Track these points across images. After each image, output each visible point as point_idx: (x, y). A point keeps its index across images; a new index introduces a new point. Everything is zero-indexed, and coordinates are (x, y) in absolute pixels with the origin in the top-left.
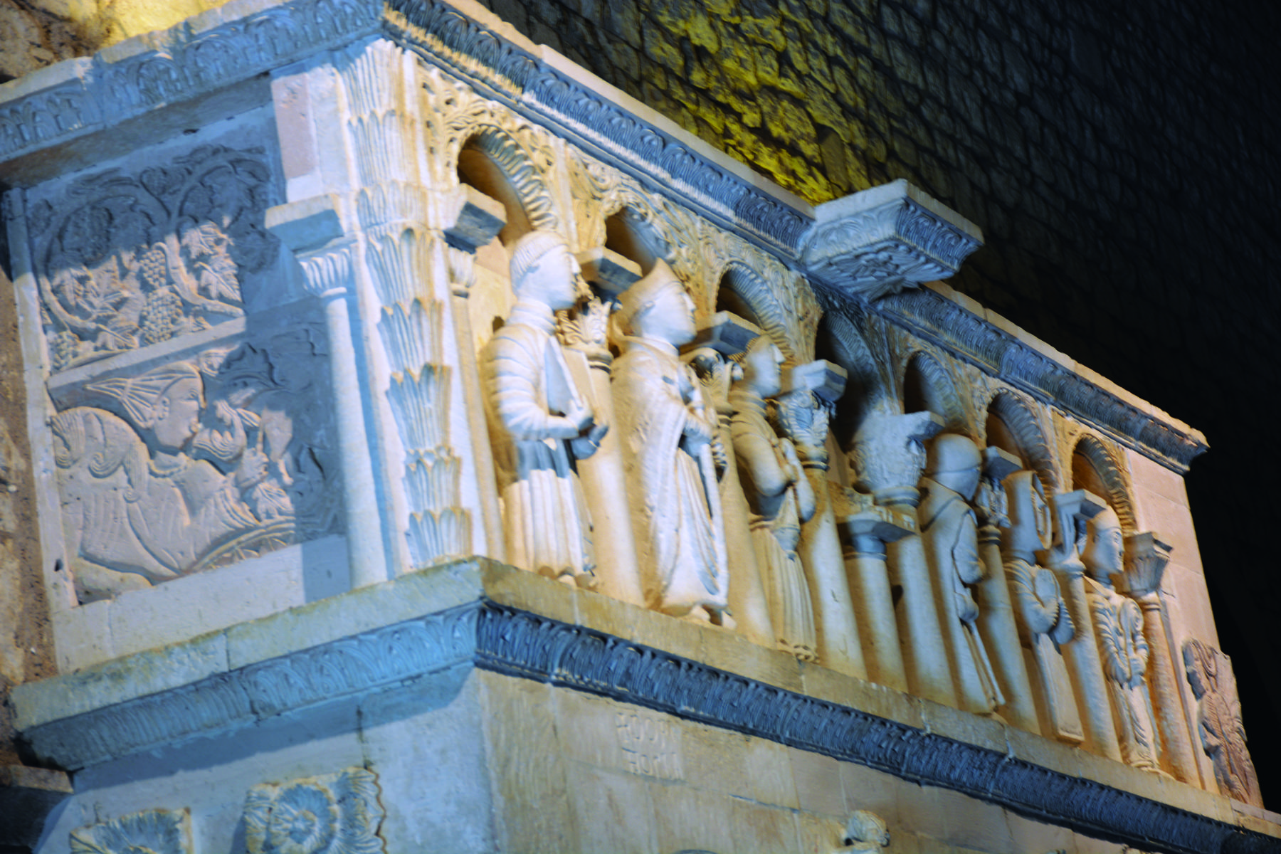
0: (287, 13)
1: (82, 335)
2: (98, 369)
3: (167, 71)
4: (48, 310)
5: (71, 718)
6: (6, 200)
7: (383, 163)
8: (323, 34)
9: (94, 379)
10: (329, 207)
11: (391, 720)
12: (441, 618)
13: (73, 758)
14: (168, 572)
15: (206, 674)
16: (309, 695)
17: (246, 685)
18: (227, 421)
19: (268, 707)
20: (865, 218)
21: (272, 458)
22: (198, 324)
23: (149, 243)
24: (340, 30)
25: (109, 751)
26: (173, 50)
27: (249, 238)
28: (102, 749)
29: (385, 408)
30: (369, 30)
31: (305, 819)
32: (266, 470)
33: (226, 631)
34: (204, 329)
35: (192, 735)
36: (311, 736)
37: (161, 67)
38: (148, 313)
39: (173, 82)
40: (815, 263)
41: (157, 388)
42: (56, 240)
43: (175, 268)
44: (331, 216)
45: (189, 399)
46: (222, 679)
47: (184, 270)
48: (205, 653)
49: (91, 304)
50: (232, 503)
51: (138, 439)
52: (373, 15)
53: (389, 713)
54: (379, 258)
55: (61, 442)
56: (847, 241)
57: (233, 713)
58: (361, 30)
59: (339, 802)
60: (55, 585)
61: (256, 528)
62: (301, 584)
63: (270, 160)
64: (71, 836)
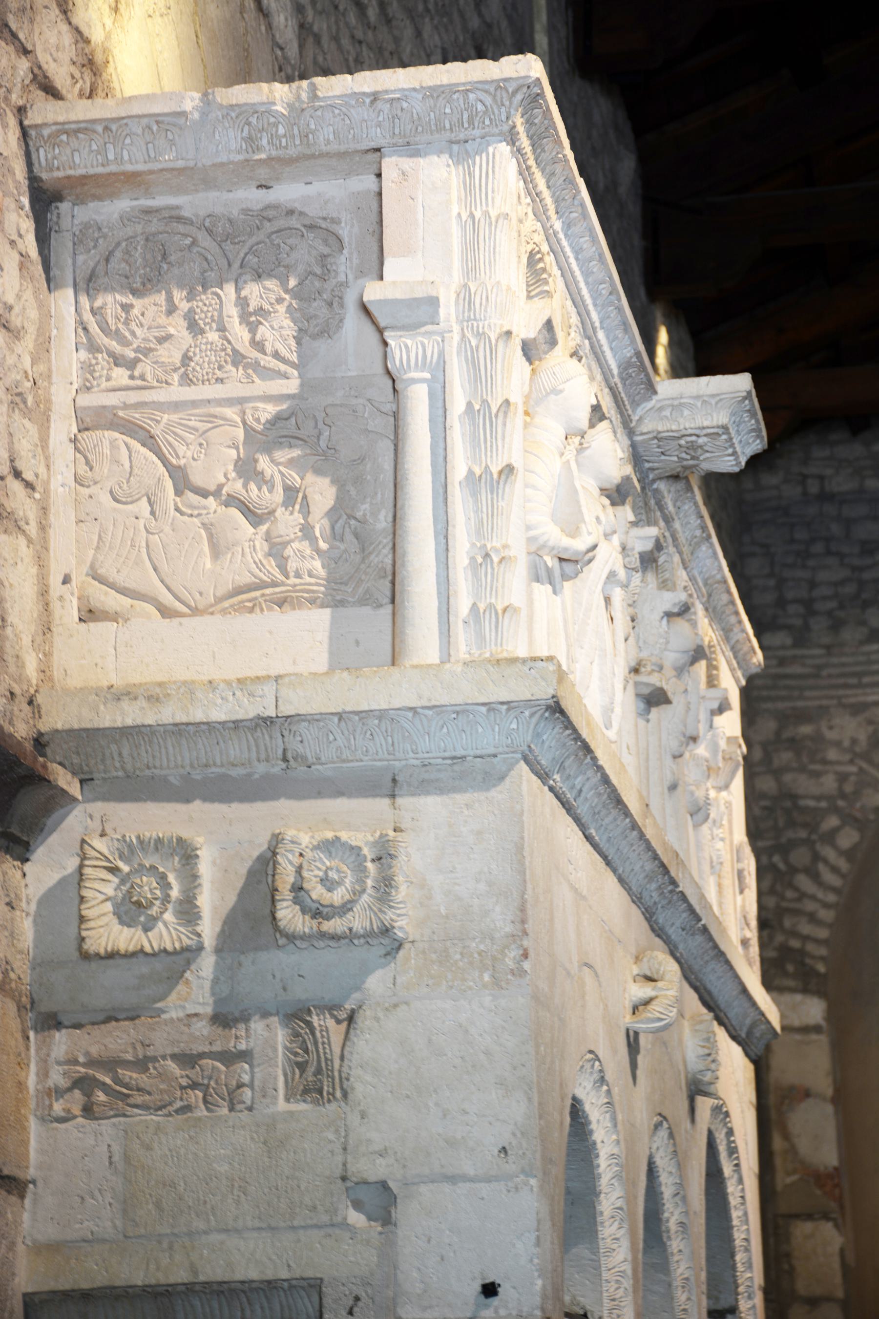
0: (420, 96)
1: (117, 361)
2: (133, 397)
3: (276, 125)
4: (85, 329)
5: (98, 729)
6: (55, 212)
7: (490, 262)
8: (448, 126)
9: (126, 406)
10: (434, 294)
11: (428, 793)
12: (505, 707)
13: (85, 768)
14: (185, 610)
15: (251, 715)
16: (346, 754)
17: (286, 733)
18: (268, 477)
19: (300, 758)
20: (704, 402)
21: (309, 520)
22: (248, 376)
23: (205, 288)
24: (466, 125)
25: (123, 768)
26: (290, 106)
27: (315, 304)
28: (118, 765)
29: (458, 497)
30: (496, 130)
31: (338, 871)
32: (301, 531)
33: (277, 678)
34: (253, 382)
35: (214, 769)
36: (340, 793)
37: (272, 120)
38: (195, 354)
39: (279, 138)
40: (642, 434)
41: (196, 430)
42: (103, 263)
43: (229, 317)
44: (433, 302)
45: (229, 447)
46: (266, 722)
47: (237, 320)
48: (252, 695)
49: (133, 333)
50: (260, 555)
51: (166, 474)
52: (504, 118)
53: (425, 787)
54: (472, 352)
55: (83, 460)
56: (681, 420)
57: (263, 756)
58: (487, 130)
59: (373, 860)
60: (61, 598)
61: (283, 584)
62: (326, 646)
63: (346, 232)
64: (83, 841)
